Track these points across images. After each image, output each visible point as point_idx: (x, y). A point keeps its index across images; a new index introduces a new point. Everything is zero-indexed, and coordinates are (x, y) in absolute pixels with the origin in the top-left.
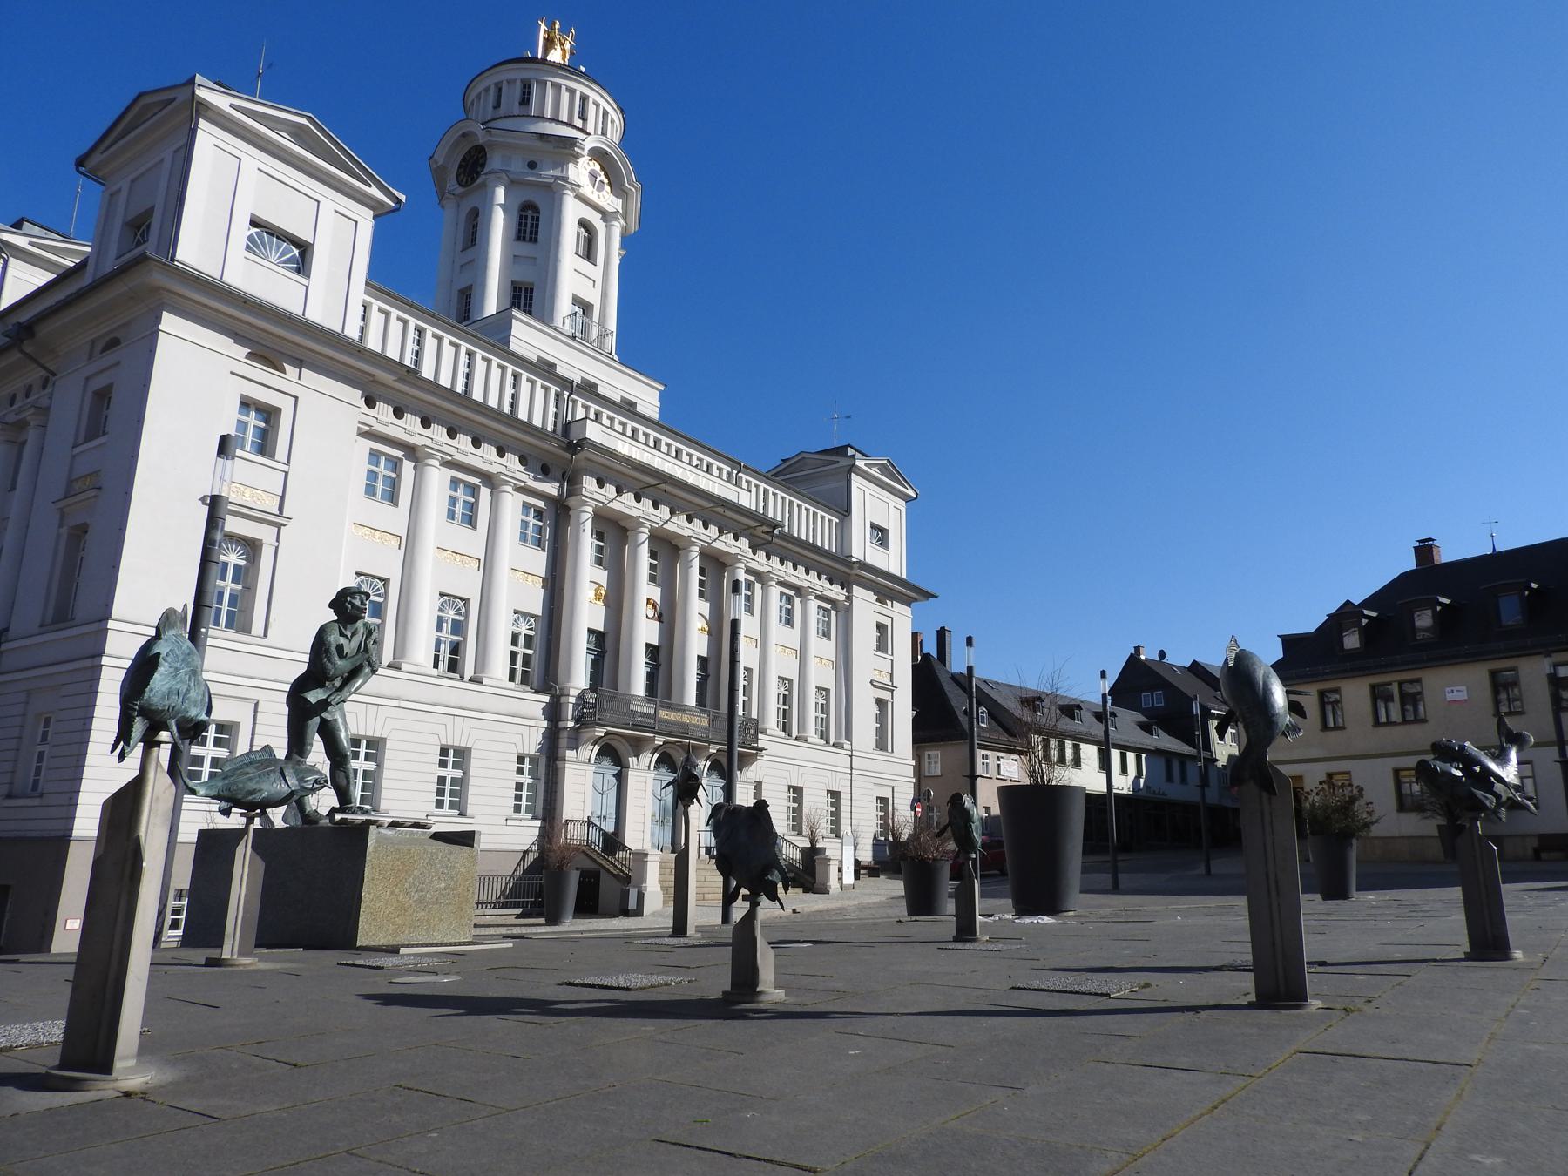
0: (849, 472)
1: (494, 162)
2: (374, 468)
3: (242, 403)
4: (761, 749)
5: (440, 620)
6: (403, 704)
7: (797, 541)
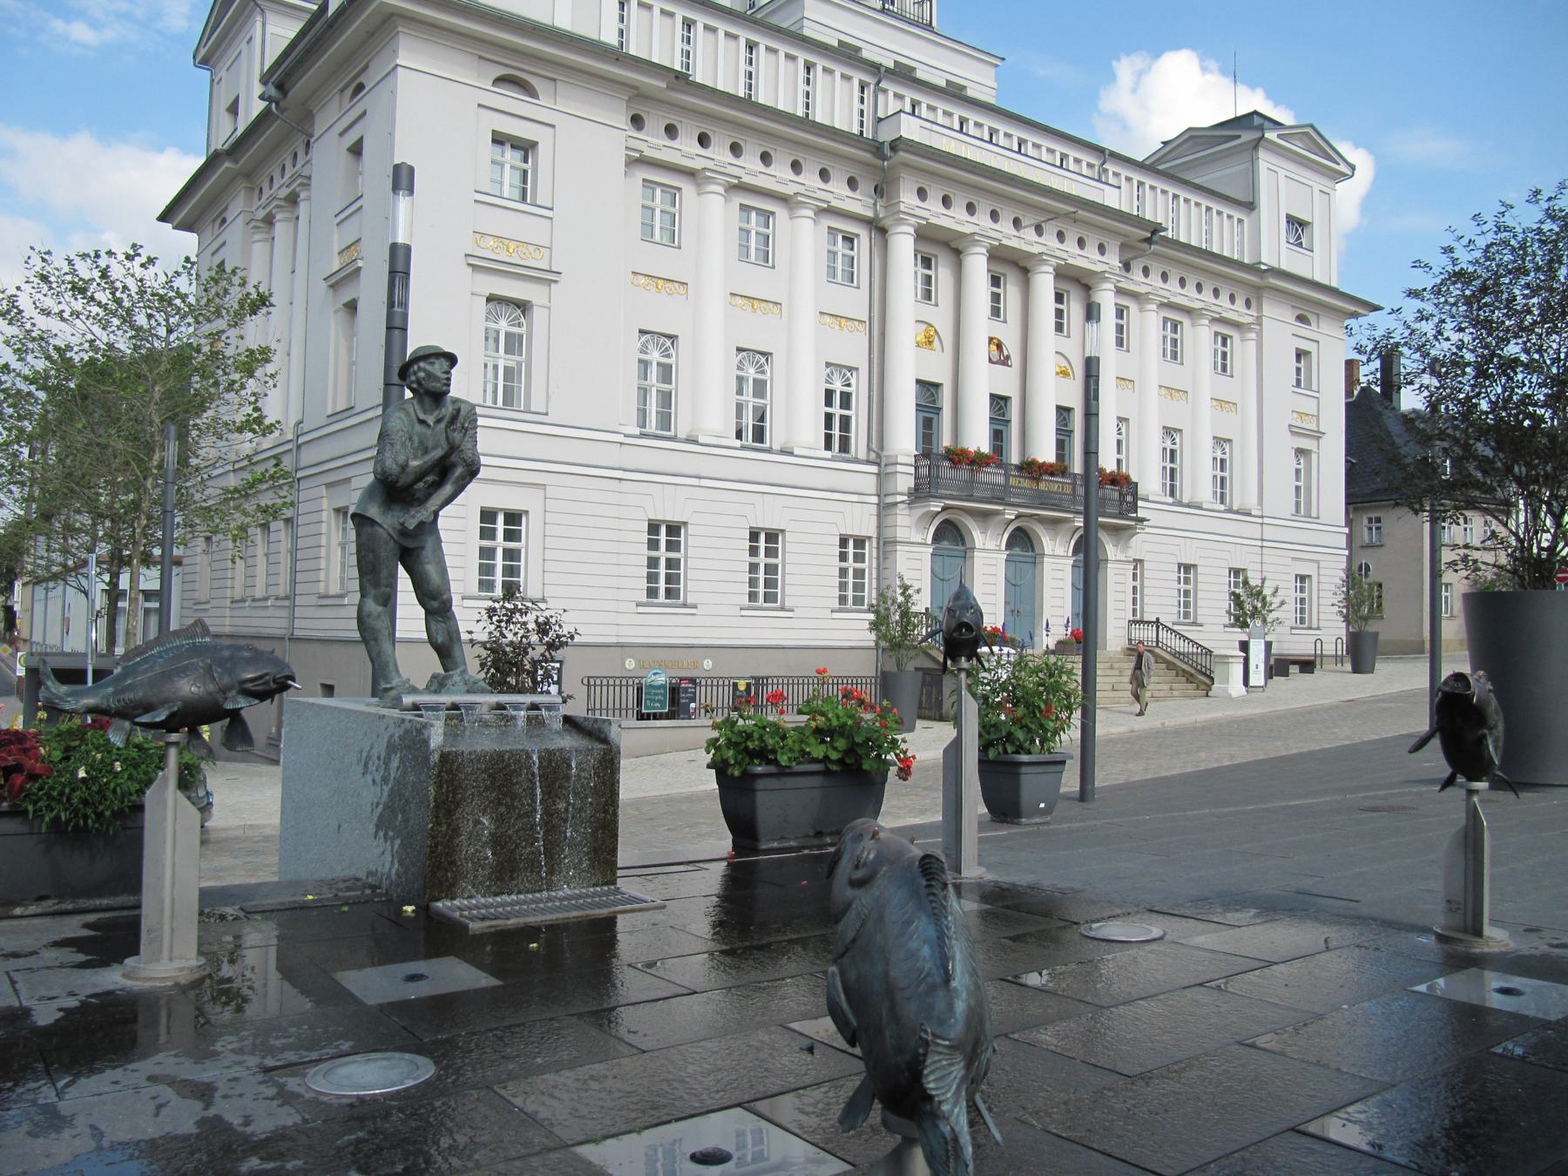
0: (1256, 147)
2: (995, 290)
3: (494, 141)
4: (1142, 520)
5: (740, 380)
6: (705, 482)
7: (1187, 248)
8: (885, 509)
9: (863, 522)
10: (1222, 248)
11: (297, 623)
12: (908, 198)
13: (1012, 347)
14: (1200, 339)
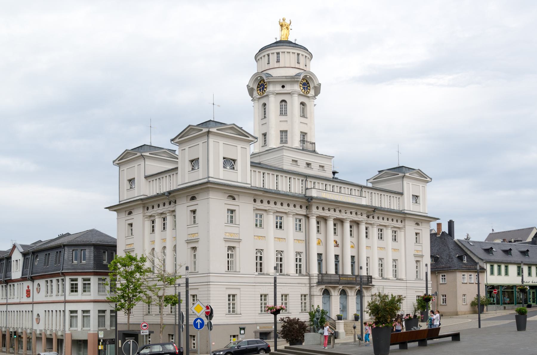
1: (271, 88)
4: (373, 286)
8: (310, 287)
9: (306, 291)
10: (385, 205)
11: (164, 321)
12: (314, 210)
13: (339, 242)
14: (388, 234)
